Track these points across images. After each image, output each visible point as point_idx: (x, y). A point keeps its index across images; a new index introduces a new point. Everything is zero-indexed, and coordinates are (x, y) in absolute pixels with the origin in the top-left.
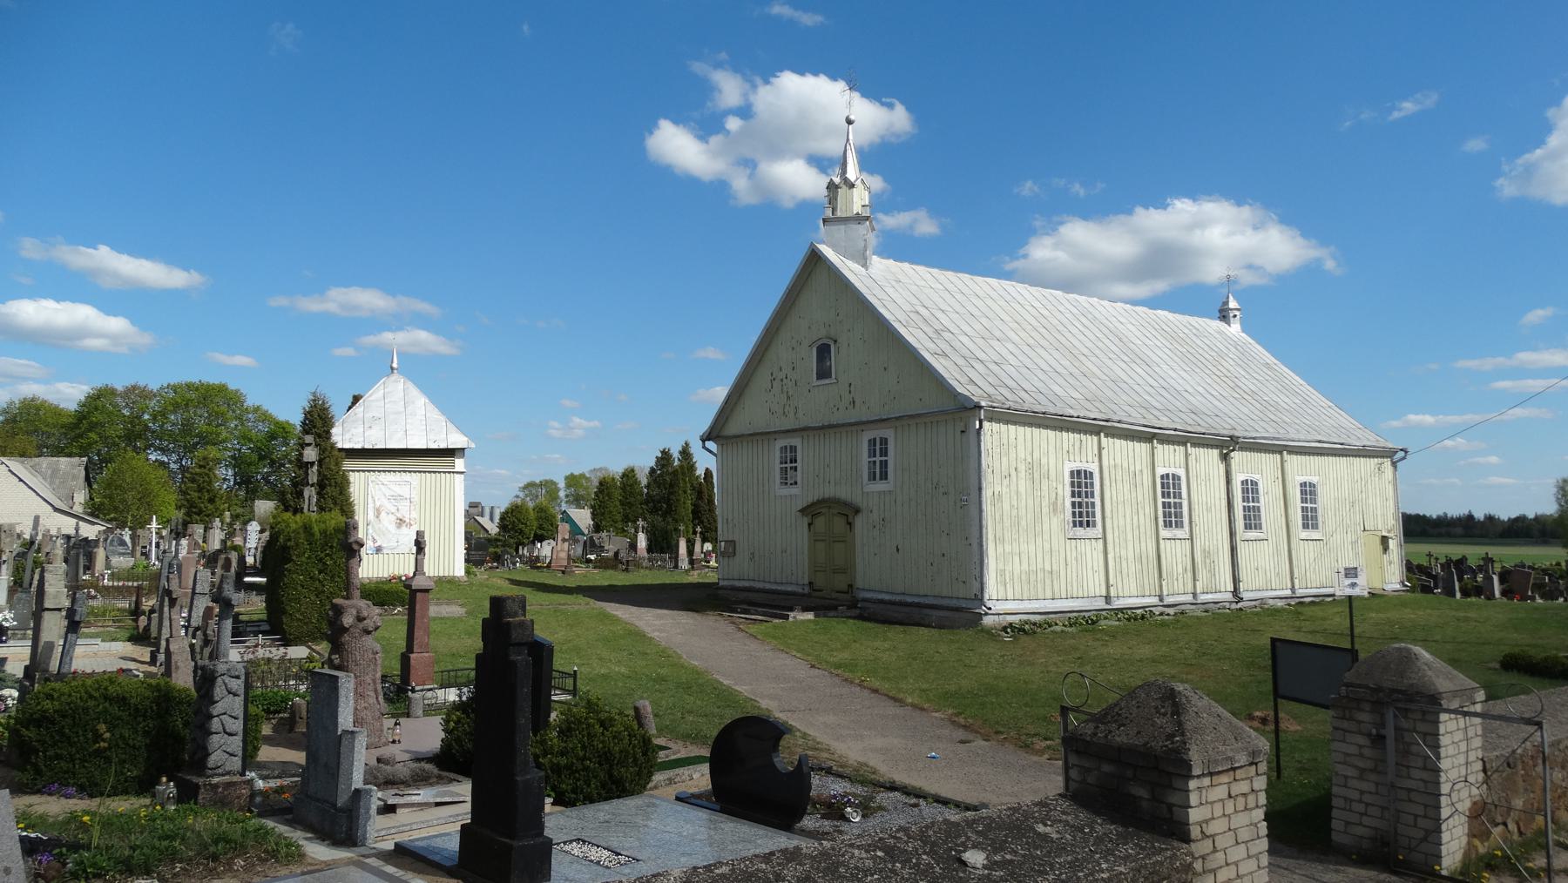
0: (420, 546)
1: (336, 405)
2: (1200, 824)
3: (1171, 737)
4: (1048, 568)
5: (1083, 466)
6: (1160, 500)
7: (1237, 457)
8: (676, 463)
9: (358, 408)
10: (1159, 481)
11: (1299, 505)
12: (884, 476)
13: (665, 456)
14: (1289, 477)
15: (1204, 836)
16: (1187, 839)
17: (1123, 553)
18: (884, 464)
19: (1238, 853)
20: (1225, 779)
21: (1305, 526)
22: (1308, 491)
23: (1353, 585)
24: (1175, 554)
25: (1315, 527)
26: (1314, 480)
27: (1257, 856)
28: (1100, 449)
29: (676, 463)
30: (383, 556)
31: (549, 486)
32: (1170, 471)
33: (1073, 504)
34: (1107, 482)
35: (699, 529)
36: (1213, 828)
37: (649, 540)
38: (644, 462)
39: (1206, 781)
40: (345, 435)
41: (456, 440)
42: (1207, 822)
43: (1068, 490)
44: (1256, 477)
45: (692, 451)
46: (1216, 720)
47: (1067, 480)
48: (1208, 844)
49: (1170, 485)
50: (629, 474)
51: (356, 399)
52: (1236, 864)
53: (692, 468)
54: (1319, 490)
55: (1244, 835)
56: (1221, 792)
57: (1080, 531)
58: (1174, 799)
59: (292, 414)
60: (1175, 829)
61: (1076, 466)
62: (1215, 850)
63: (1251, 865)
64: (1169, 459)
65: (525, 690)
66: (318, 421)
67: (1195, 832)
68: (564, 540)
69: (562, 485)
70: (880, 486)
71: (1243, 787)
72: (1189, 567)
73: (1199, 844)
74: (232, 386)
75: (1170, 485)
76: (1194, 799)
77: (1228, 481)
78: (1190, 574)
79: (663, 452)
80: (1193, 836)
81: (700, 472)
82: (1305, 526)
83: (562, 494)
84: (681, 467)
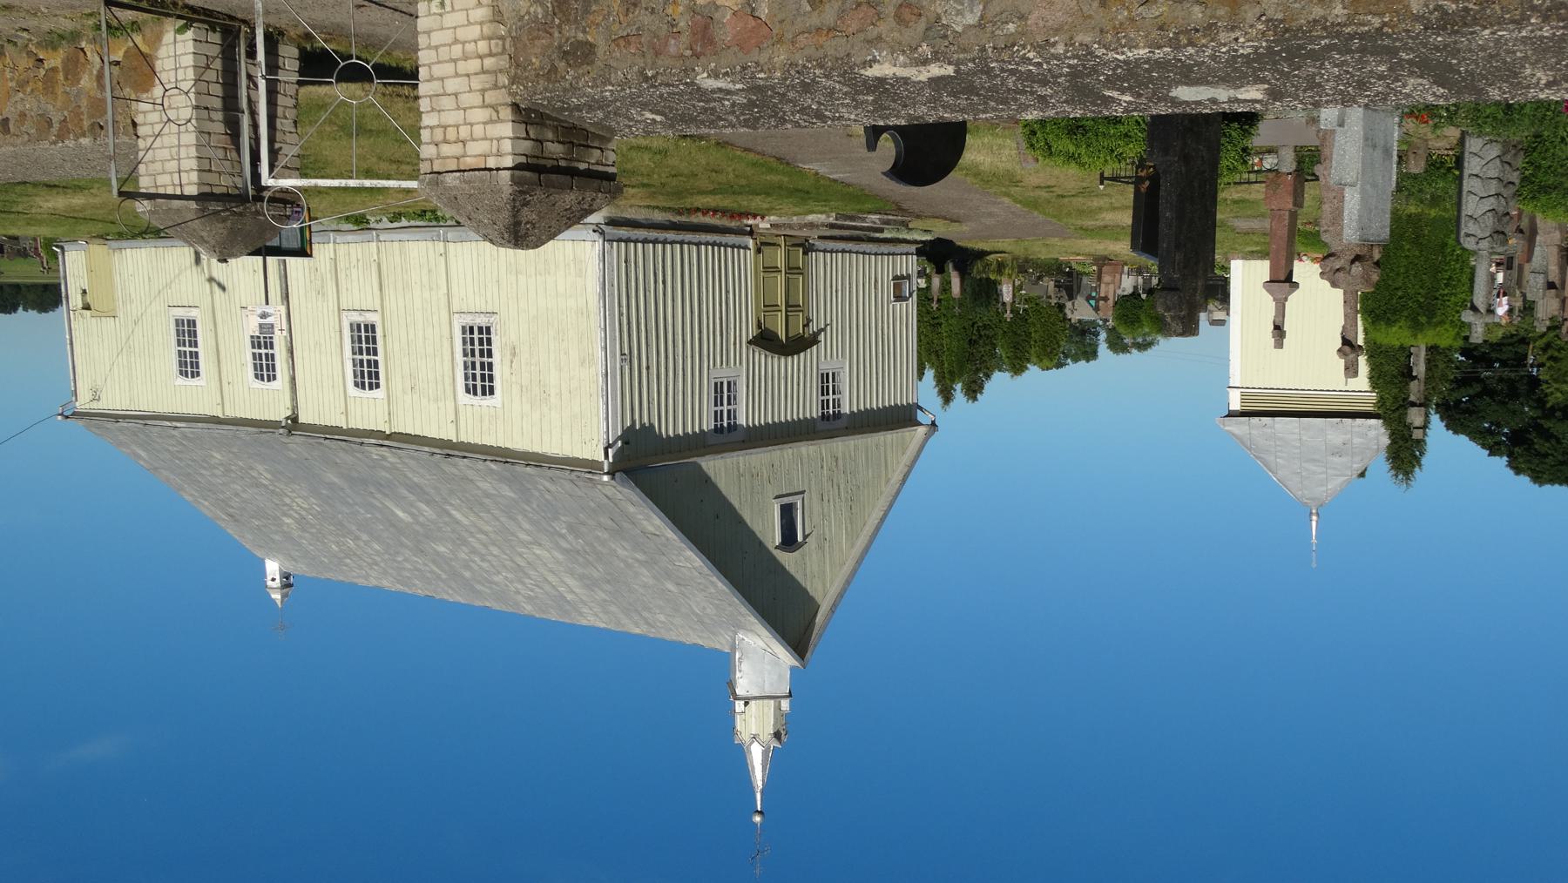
0: (1279, 330)
1: (1381, 467)
2: (499, 120)
3: (526, 204)
4: (522, 278)
5: (478, 400)
6: (380, 358)
7: (280, 413)
8: (958, 387)
9: (1358, 467)
10: (382, 381)
11: (201, 349)
12: (718, 388)
13: (973, 391)
14: (215, 384)
15: (494, 107)
16: (515, 107)
17: (427, 295)
18: (718, 401)
19: (452, 85)
20: (470, 162)
21: (192, 323)
22: (189, 366)
23: (264, 316)
24: (361, 295)
25: (179, 323)
26: (181, 381)
27: (431, 79)
28: (456, 422)
29: (958, 387)
30: (1321, 306)
31: (1117, 345)
32: (368, 393)
33: (490, 355)
34: (448, 381)
35: (935, 306)
36: (480, 115)
37: (999, 295)
38: (999, 382)
39: (491, 163)
40: (1376, 433)
41: (1241, 427)
42: (491, 121)
43: (496, 372)
44: (258, 384)
45: (939, 400)
46: (473, 215)
47: (497, 384)
48: (491, 97)
49: (368, 376)
50: (1018, 369)
51: (1362, 475)
52: (457, 75)
53: (940, 379)
54: (176, 367)
55: (447, 102)
56: (475, 148)
57: (481, 321)
58: (526, 146)
59: (1446, 447)
60: (527, 116)
61: (488, 401)
62: (483, 91)
63: (438, 71)
64: (368, 411)
65: (1167, 214)
66: (1405, 454)
67: (506, 113)
68: (1106, 299)
69: (1103, 349)
70: (723, 374)
71: (447, 150)
72: (342, 276)
73: (501, 101)
74: (1524, 480)
75: (368, 376)
76: (507, 146)
77: (293, 379)
78: (341, 265)
79: (975, 399)
80: (509, 110)
81: (930, 374)
82: (192, 323)
83: (1103, 336)
84: (953, 381)
